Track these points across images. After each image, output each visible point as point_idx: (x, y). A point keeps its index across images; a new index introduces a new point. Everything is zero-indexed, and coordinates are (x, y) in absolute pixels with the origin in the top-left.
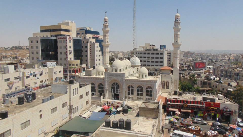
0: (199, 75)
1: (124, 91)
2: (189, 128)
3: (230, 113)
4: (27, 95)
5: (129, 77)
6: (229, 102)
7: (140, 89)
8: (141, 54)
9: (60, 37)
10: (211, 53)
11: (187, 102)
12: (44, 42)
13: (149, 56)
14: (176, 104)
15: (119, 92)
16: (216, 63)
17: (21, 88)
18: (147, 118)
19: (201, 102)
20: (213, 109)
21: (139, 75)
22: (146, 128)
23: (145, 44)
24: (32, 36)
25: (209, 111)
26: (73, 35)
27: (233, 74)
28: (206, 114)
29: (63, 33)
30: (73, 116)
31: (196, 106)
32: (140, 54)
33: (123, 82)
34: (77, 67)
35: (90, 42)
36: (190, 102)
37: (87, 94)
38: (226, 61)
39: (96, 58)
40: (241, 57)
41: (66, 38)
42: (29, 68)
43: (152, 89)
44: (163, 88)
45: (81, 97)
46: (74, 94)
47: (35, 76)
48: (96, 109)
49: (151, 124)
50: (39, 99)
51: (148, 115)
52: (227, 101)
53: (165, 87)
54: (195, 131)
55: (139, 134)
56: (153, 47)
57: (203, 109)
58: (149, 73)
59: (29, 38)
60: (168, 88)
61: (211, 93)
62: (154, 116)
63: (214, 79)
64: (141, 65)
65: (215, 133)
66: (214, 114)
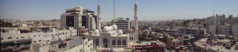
0: (146, 32)
4: (63, 44)
6: (162, 43)
8: (116, 23)
9: (75, 15)
11: (144, 46)
12: (68, 17)
13: (121, 24)
17: (58, 39)
21: (118, 34)
24: (62, 15)
26: (81, 13)
29: (77, 12)
34: (84, 30)
36: (146, 46)
37: (91, 45)
39: (93, 25)
41: (78, 15)
42: (61, 30)
44: (130, 40)
45: (89, 46)
47: (64, 34)
50: (68, 46)
53: (131, 40)
56: (122, 19)
59: (61, 16)
60: (133, 40)
63: (153, 33)
64: (118, 29)
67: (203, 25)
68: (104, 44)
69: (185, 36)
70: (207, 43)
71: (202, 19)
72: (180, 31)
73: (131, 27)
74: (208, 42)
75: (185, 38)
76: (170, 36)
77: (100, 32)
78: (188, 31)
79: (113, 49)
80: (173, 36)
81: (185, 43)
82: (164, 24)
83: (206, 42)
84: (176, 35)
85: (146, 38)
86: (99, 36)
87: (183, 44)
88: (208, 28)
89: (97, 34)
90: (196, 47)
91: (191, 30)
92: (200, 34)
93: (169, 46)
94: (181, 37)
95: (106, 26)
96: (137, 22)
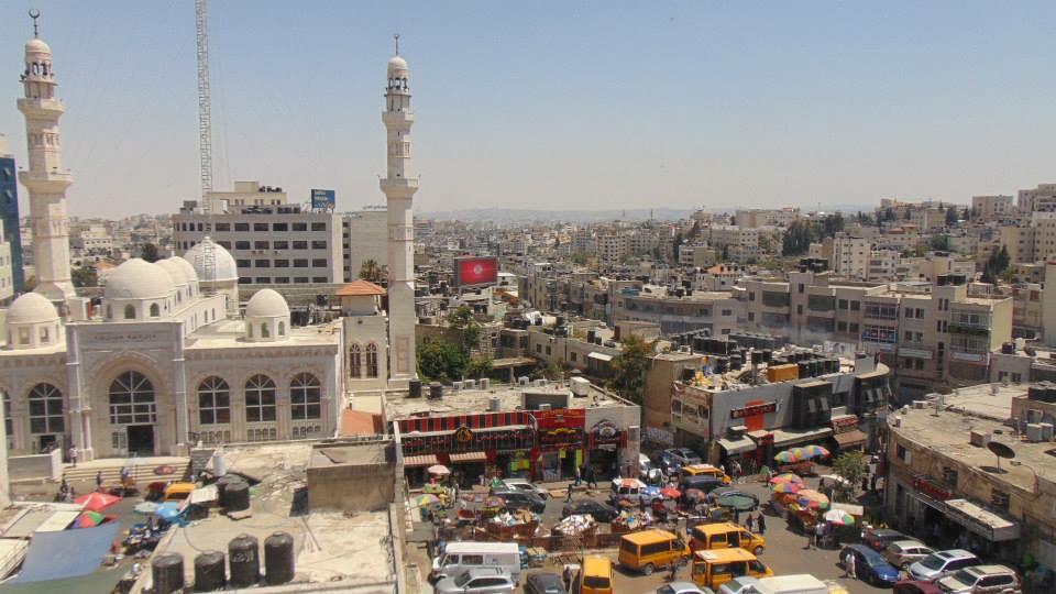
0: (481, 307)
2: (493, 524)
3: (618, 439)
6: (609, 402)
7: (305, 387)
8: (222, 227)
10: (492, 223)
11: (470, 420)
14: (429, 437)
15: (154, 416)
20: (564, 434)
21: (250, 327)
22: (356, 555)
25: (553, 443)
27: (591, 300)
28: (540, 459)
32: (256, 229)
33: (173, 370)
36: (482, 420)
44: (355, 373)
48: (48, 517)
49: (373, 535)
51: (348, 501)
52: (603, 400)
53: (364, 370)
54: (518, 528)
56: (276, 197)
57: (531, 439)
58: (292, 314)
60: (373, 372)
61: (544, 373)
62: (375, 495)
63: (539, 322)
64: (242, 281)
65: (586, 521)
66: (567, 453)
67: (972, 265)
68: (122, 420)
69: (807, 356)
70: (1018, 425)
71: (963, 200)
72: (758, 307)
73: (356, 269)
74: (1030, 417)
75: (802, 367)
76: (674, 348)
77: (62, 314)
78: (829, 314)
79: (216, 460)
80: (701, 346)
81: (804, 411)
82: (619, 247)
83: (1006, 423)
84: (725, 339)
85: (474, 353)
86: (61, 359)
87: (780, 418)
88: (1034, 296)
89: (37, 336)
90: (908, 455)
91: (856, 306)
92: (941, 345)
93: (666, 425)
94: (767, 357)
96: (409, 222)
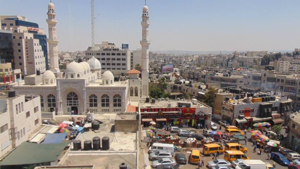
0: (168, 78)
1: (85, 103)
3: (205, 117)
5: (89, 83)
6: (203, 106)
7: (105, 98)
8: (98, 54)
10: (174, 54)
11: (162, 109)
13: (108, 57)
14: (150, 114)
15: (78, 104)
16: (181, 64)
18: (125, 133)
19: (176, 108)
21: (103, 81)
22: (127, 144)
23: (102, 42)
27: (200, 77)
28: (182, 121)
30: (18, 143)
31: (172, 113)
34: (8, 74)
35: (25, 38)
36: (166, 110)
37: (36, 110)
38: (189, 62)
39: (36, 60)
40: (203, 58)
43: (120, 97)
44: (132, 95)
45: (28, 114)
46: (21, 109)
48: (51, 129)
49: (131, 139)
51: (126, 129)
52: (201, 105)
53: (134, 94)
54: (174, 140)
55: (121, 153)
56: (113, 46)
58: (115, 78)
60: (137, 95)
62: (133, 129)
63: (184, 83)
64: (103, 69)
65: (194, 140)
68: (70, 105)
69: (265, 95)
73: (134, 66)
76: (224, 92)
77: (56, 76)
79: (91, 116)
80: (232, 91)
81: (263, 112)
82: (210, 62)
86: (55, 88)
87: (255, 113)
89: (50, 82)
90: (296, 127)
91: (282, 81)
93: (220, 114)
94: (252, 95)
95: (72, 61)
96: (148, 53)
